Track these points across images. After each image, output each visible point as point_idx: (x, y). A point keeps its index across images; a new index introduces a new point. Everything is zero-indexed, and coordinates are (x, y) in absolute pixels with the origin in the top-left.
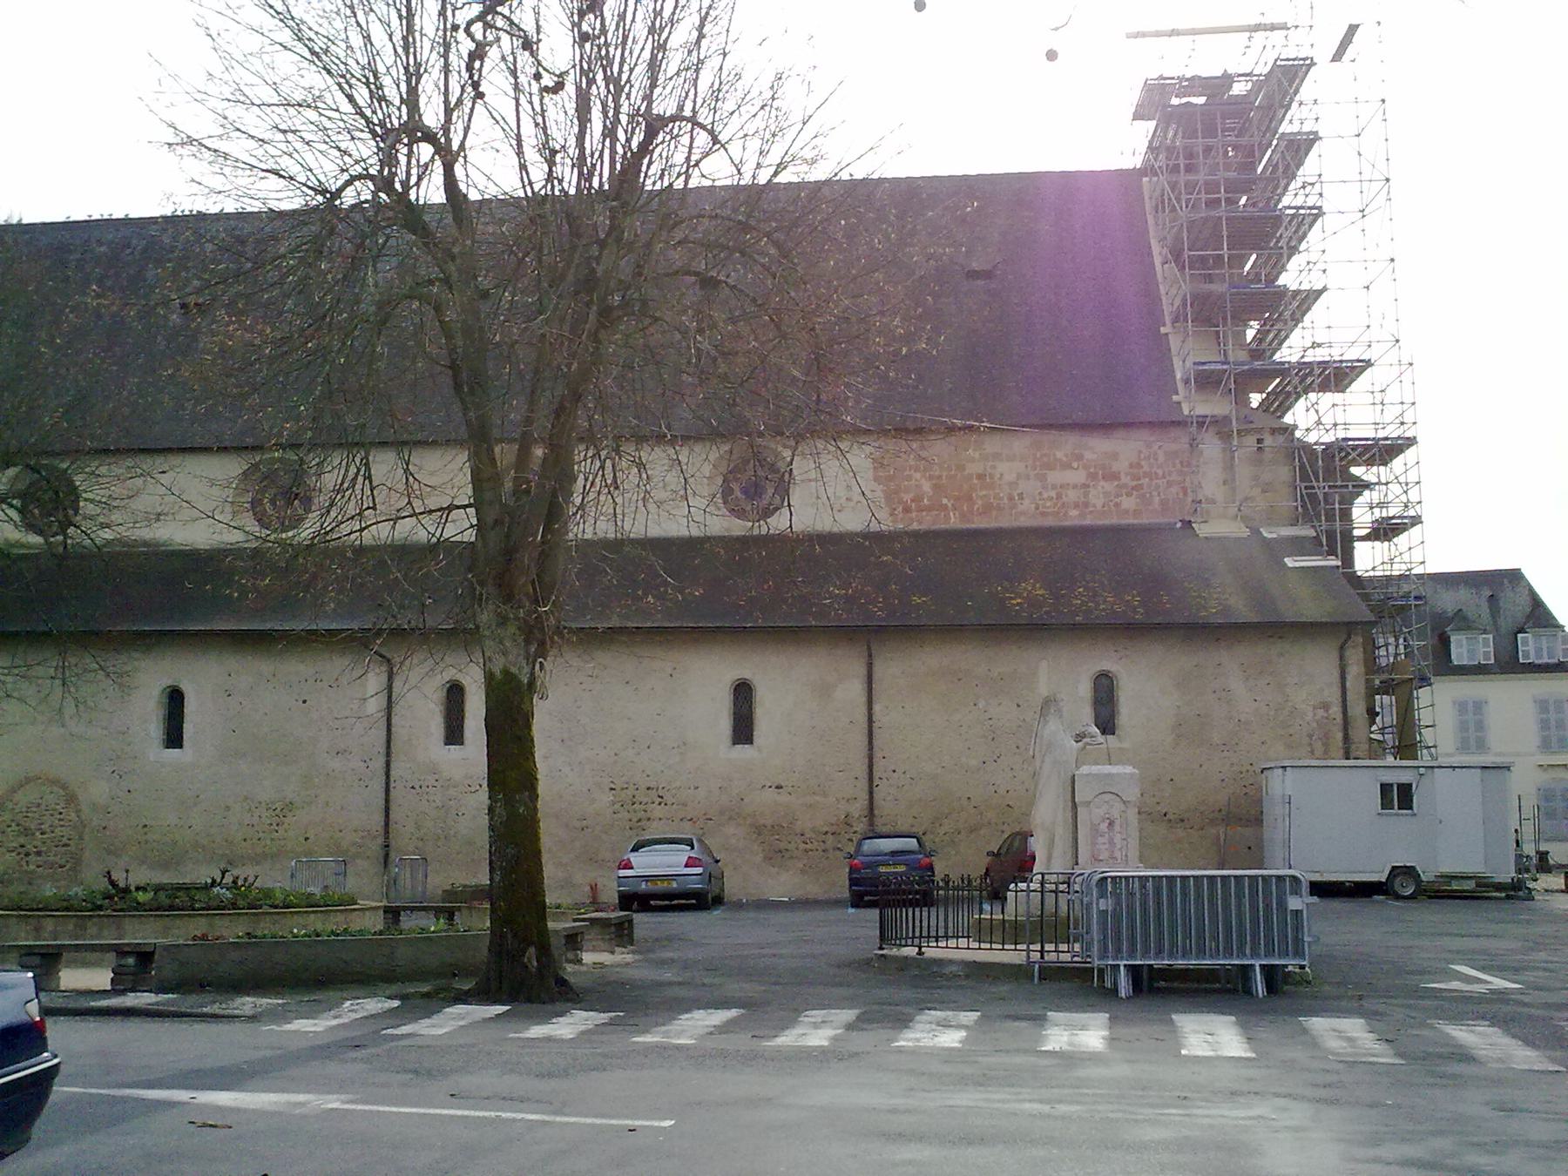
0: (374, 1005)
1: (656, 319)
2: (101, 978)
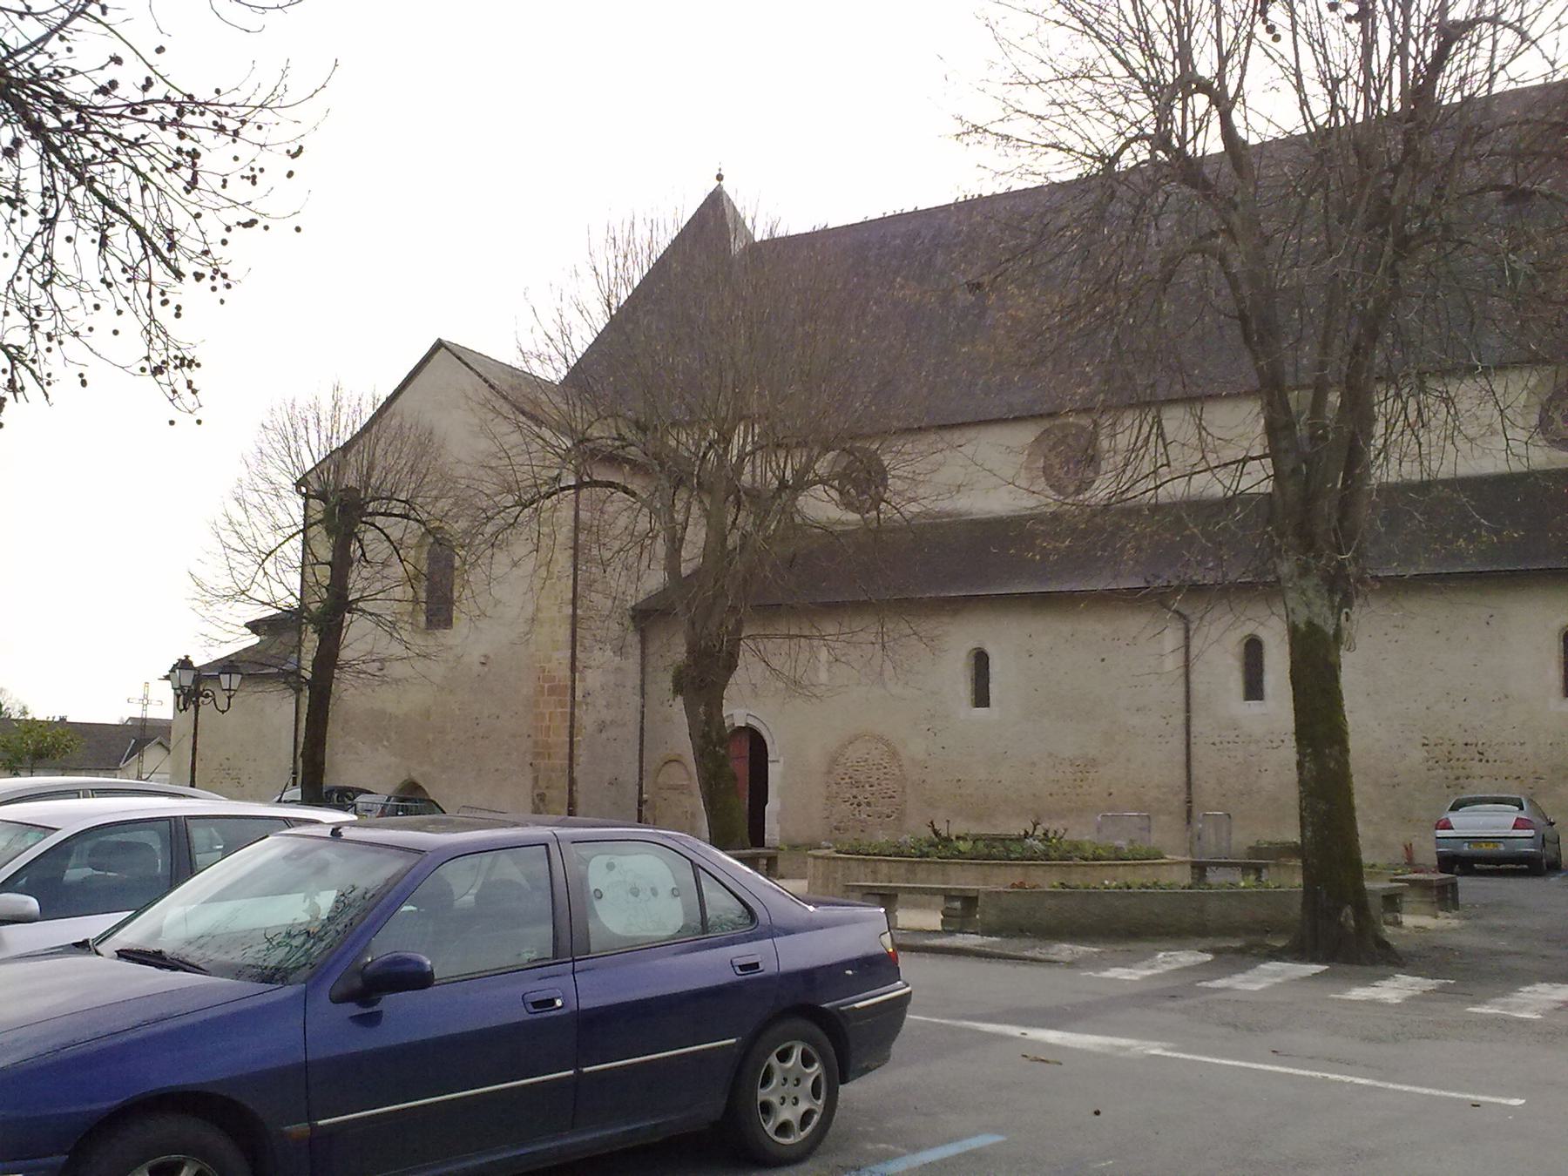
0: (1188, 957)
1: (1461, 243)
2: (933, 920)
